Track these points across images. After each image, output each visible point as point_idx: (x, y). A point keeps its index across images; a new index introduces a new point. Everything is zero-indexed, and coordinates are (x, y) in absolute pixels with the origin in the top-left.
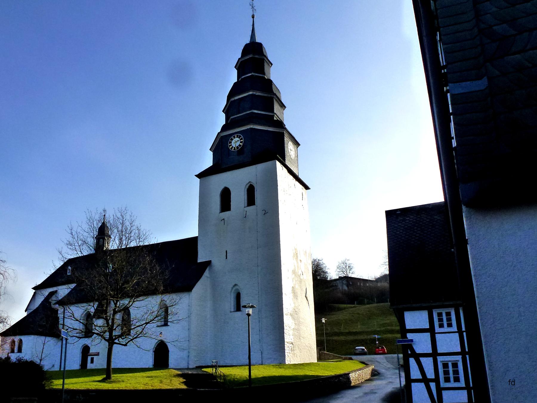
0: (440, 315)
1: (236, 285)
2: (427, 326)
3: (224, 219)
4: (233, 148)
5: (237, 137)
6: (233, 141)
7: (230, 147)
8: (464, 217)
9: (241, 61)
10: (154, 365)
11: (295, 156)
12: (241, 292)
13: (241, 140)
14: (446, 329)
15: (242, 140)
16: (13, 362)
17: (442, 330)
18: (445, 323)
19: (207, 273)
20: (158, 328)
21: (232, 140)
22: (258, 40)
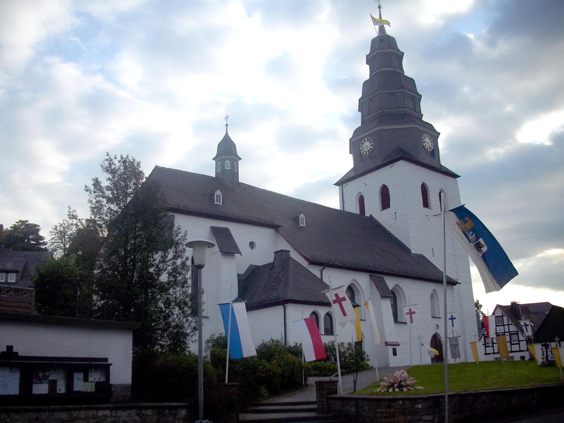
2: (512, 346)
4: (365, 152)
8: (34, 407)
13: (371, 143)
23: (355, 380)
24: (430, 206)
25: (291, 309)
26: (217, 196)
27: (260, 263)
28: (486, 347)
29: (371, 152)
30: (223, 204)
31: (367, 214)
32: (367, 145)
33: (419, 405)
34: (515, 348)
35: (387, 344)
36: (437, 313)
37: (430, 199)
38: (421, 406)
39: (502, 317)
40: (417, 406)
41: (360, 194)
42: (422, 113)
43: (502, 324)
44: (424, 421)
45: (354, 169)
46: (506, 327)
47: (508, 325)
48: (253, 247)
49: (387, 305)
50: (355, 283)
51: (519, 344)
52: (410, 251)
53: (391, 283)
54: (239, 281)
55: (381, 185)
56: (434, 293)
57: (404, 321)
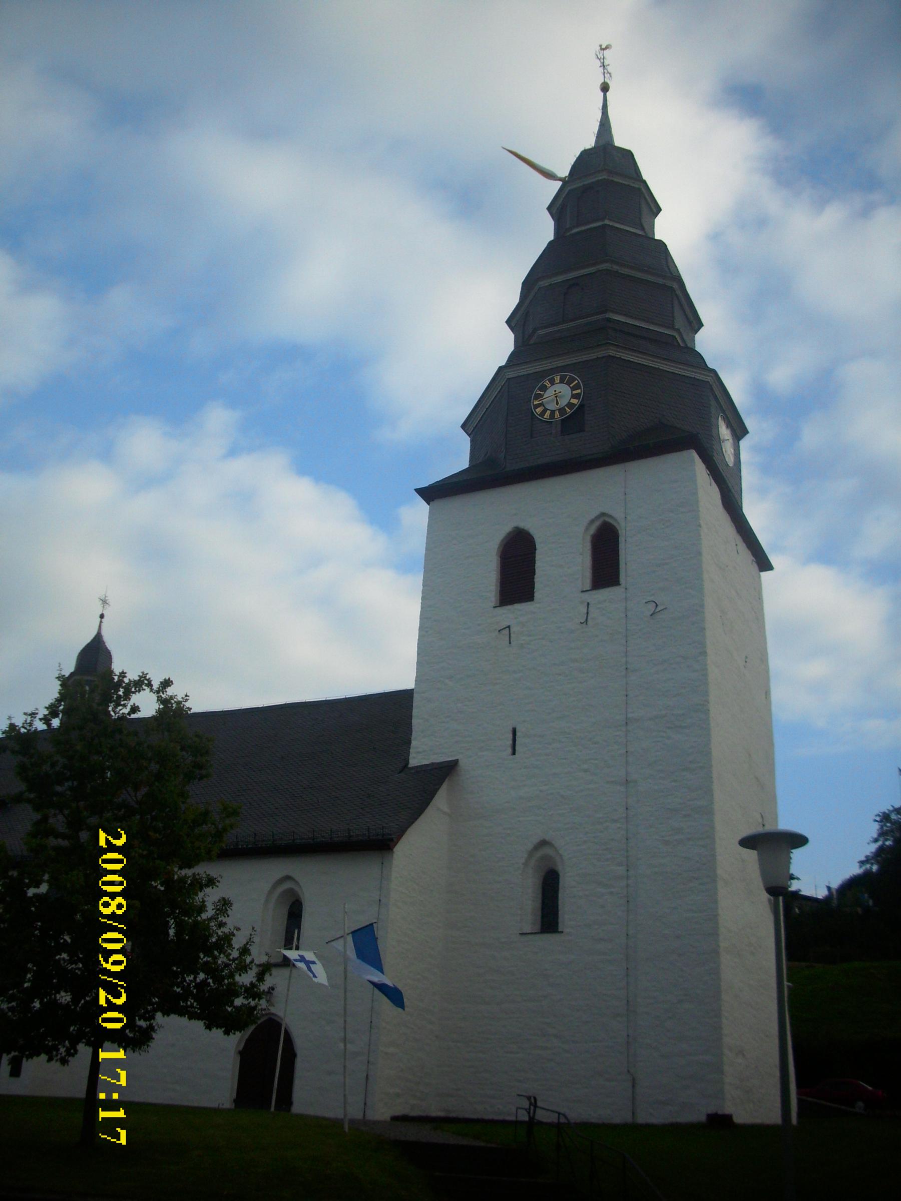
1: (544, 843)
3: (509, 627)
4: (548, 413)
5: (562, 381)
6: (550, 393)
7: (537, 410)
9: (569, 188)
10: (235, 1101)
11: (735, 465)
12: (560, 868)
15: (579, 391)
16: (791, 854)
19: (441, 800)
20: (583, 594)
21: (544, 388)
22: (620, 140)
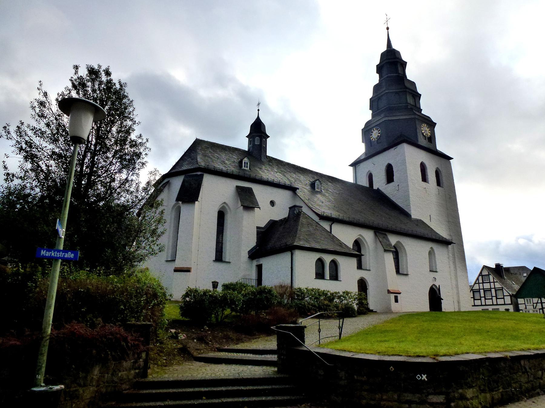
0: (527, 300)
2: (497, 300)
14: (529, 304)
17: (528, 304)
18: (529, 302)
21: (372, 132)
23: (341, 325)
24: (428, 181)
25: (298, 254)
26: (245, 163)
27: (277, 218)
28: (474, 300)
29: (379, 138)
30: (250, 169)
31: (375, 187)
32: (375, 134)
33: (423, 375)
34: (500, 301)
35: (389, 292)
36: (434, 268)
37: (427, 175)
38: (426, 377)
39: (488, 276)
40: (419, 377)
41: (369, 172)
42: (421, 108)
43: (489, 281)
44: (432, 404)
45: (366, 153)
46: (492, 284)
47: (494, 282)
48: (274, 205)
49: (389, 258)
50: (361, 238)
51: (504, 298)
52: (411, 216)
53: (393, 240)
54: (258, 233)
55: (386, 164)
56: (432, 252)
57: (405, 273)
